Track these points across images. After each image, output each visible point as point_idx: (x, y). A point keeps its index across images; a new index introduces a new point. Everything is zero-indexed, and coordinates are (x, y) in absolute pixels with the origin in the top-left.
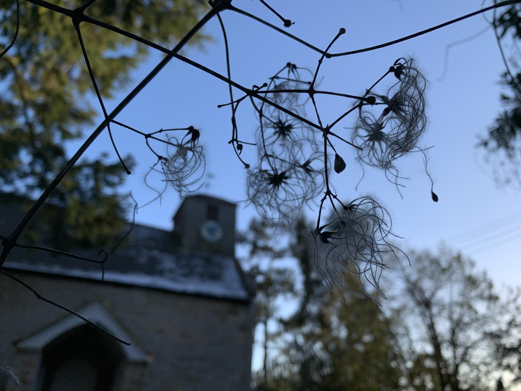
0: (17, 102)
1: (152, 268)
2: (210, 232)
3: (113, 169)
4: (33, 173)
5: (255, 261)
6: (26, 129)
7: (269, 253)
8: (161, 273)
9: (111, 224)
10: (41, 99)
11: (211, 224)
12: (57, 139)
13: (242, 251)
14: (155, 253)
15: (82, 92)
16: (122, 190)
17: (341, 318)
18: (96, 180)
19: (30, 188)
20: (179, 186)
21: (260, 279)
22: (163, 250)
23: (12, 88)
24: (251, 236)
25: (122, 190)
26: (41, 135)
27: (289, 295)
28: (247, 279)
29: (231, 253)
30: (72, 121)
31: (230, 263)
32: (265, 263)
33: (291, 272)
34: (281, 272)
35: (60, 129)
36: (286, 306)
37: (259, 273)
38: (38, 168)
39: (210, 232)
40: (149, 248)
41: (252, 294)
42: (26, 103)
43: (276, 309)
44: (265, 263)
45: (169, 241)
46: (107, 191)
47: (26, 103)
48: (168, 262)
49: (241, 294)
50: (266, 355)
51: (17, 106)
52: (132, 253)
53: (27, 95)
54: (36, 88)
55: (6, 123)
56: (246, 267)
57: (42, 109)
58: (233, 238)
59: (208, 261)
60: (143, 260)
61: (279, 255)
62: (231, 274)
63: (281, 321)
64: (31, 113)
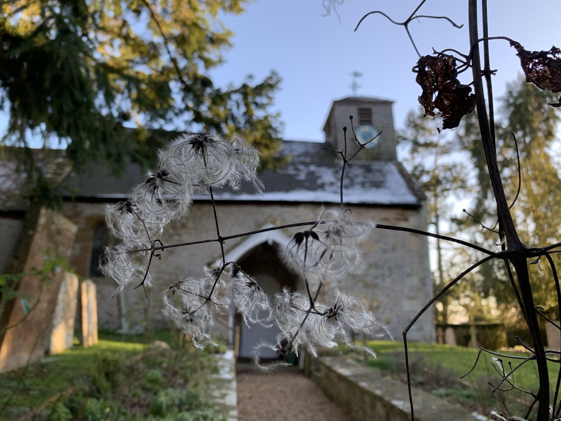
0: (158, 40)
1: (312, 183)
2: (365, 135)
3: (260, 89)
4: (187, 108)
5: (418, 160)
6: (171, 65)
7: (434, 150)
8: (322, 187)
9: (267, 146)
10: (176, 31)
11: (366, 129)
12: (201, 71)
13: (403, 152)
14: (313, 168)
15: (214, 13)
16: (271, 110)
17: (527, 212)
18: (247, 105)
19: (189, 123)
20: (427, 111)
21: (425, 179)
22: (319, 165)
23: (149, 26)
24: (410, 133)
25: (271, 110)
26: (185, 68)
27: (461, 192)
28: (410, 179)
29: (392, 158)
30: (209, 47)
31: (392, 167)
32: (428, 161)
33: (463, 167)
34: (449, 169)
35: (201, 57)
36: (459, 203)
37: (423, 172)
38: (191, 104)
39: (365, 135)
40: (306, 164)
41: (422, 198)
42: (167, 39)
43: (448, 208)
44: (428, 161)
45: (326, 153)
46: (258, 114)
47: (167, 39)
48: (327, 175)
49: (410, 199)
50: (440, 256)
51: (159, 44)
52: (291, 171)
53: (165, 30)
54: (168, 20)
55: (153, 64)
56: (409, 168)
57: (181, 41)
58: (391, 138)
59: (368, 169)
60: (302, 176)
61: (446, 151)
62: (395, 180)
63: (454, 220)
64: (172, 47)
